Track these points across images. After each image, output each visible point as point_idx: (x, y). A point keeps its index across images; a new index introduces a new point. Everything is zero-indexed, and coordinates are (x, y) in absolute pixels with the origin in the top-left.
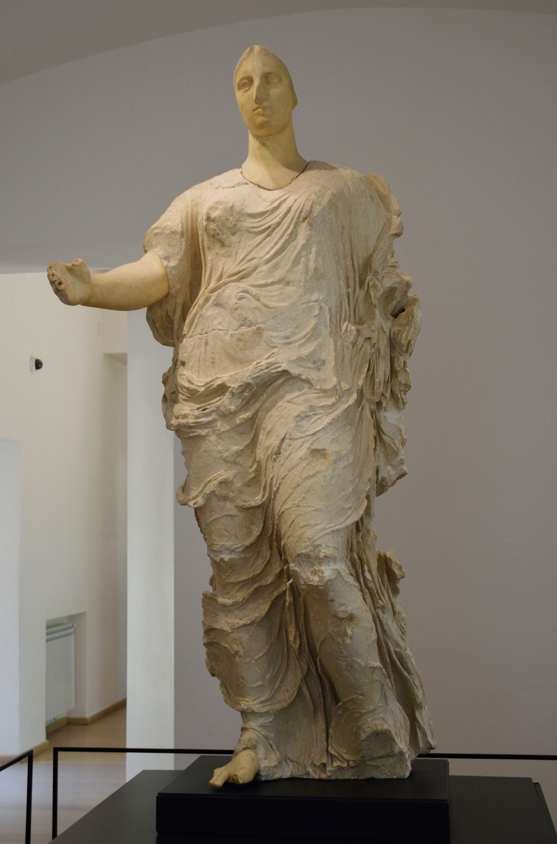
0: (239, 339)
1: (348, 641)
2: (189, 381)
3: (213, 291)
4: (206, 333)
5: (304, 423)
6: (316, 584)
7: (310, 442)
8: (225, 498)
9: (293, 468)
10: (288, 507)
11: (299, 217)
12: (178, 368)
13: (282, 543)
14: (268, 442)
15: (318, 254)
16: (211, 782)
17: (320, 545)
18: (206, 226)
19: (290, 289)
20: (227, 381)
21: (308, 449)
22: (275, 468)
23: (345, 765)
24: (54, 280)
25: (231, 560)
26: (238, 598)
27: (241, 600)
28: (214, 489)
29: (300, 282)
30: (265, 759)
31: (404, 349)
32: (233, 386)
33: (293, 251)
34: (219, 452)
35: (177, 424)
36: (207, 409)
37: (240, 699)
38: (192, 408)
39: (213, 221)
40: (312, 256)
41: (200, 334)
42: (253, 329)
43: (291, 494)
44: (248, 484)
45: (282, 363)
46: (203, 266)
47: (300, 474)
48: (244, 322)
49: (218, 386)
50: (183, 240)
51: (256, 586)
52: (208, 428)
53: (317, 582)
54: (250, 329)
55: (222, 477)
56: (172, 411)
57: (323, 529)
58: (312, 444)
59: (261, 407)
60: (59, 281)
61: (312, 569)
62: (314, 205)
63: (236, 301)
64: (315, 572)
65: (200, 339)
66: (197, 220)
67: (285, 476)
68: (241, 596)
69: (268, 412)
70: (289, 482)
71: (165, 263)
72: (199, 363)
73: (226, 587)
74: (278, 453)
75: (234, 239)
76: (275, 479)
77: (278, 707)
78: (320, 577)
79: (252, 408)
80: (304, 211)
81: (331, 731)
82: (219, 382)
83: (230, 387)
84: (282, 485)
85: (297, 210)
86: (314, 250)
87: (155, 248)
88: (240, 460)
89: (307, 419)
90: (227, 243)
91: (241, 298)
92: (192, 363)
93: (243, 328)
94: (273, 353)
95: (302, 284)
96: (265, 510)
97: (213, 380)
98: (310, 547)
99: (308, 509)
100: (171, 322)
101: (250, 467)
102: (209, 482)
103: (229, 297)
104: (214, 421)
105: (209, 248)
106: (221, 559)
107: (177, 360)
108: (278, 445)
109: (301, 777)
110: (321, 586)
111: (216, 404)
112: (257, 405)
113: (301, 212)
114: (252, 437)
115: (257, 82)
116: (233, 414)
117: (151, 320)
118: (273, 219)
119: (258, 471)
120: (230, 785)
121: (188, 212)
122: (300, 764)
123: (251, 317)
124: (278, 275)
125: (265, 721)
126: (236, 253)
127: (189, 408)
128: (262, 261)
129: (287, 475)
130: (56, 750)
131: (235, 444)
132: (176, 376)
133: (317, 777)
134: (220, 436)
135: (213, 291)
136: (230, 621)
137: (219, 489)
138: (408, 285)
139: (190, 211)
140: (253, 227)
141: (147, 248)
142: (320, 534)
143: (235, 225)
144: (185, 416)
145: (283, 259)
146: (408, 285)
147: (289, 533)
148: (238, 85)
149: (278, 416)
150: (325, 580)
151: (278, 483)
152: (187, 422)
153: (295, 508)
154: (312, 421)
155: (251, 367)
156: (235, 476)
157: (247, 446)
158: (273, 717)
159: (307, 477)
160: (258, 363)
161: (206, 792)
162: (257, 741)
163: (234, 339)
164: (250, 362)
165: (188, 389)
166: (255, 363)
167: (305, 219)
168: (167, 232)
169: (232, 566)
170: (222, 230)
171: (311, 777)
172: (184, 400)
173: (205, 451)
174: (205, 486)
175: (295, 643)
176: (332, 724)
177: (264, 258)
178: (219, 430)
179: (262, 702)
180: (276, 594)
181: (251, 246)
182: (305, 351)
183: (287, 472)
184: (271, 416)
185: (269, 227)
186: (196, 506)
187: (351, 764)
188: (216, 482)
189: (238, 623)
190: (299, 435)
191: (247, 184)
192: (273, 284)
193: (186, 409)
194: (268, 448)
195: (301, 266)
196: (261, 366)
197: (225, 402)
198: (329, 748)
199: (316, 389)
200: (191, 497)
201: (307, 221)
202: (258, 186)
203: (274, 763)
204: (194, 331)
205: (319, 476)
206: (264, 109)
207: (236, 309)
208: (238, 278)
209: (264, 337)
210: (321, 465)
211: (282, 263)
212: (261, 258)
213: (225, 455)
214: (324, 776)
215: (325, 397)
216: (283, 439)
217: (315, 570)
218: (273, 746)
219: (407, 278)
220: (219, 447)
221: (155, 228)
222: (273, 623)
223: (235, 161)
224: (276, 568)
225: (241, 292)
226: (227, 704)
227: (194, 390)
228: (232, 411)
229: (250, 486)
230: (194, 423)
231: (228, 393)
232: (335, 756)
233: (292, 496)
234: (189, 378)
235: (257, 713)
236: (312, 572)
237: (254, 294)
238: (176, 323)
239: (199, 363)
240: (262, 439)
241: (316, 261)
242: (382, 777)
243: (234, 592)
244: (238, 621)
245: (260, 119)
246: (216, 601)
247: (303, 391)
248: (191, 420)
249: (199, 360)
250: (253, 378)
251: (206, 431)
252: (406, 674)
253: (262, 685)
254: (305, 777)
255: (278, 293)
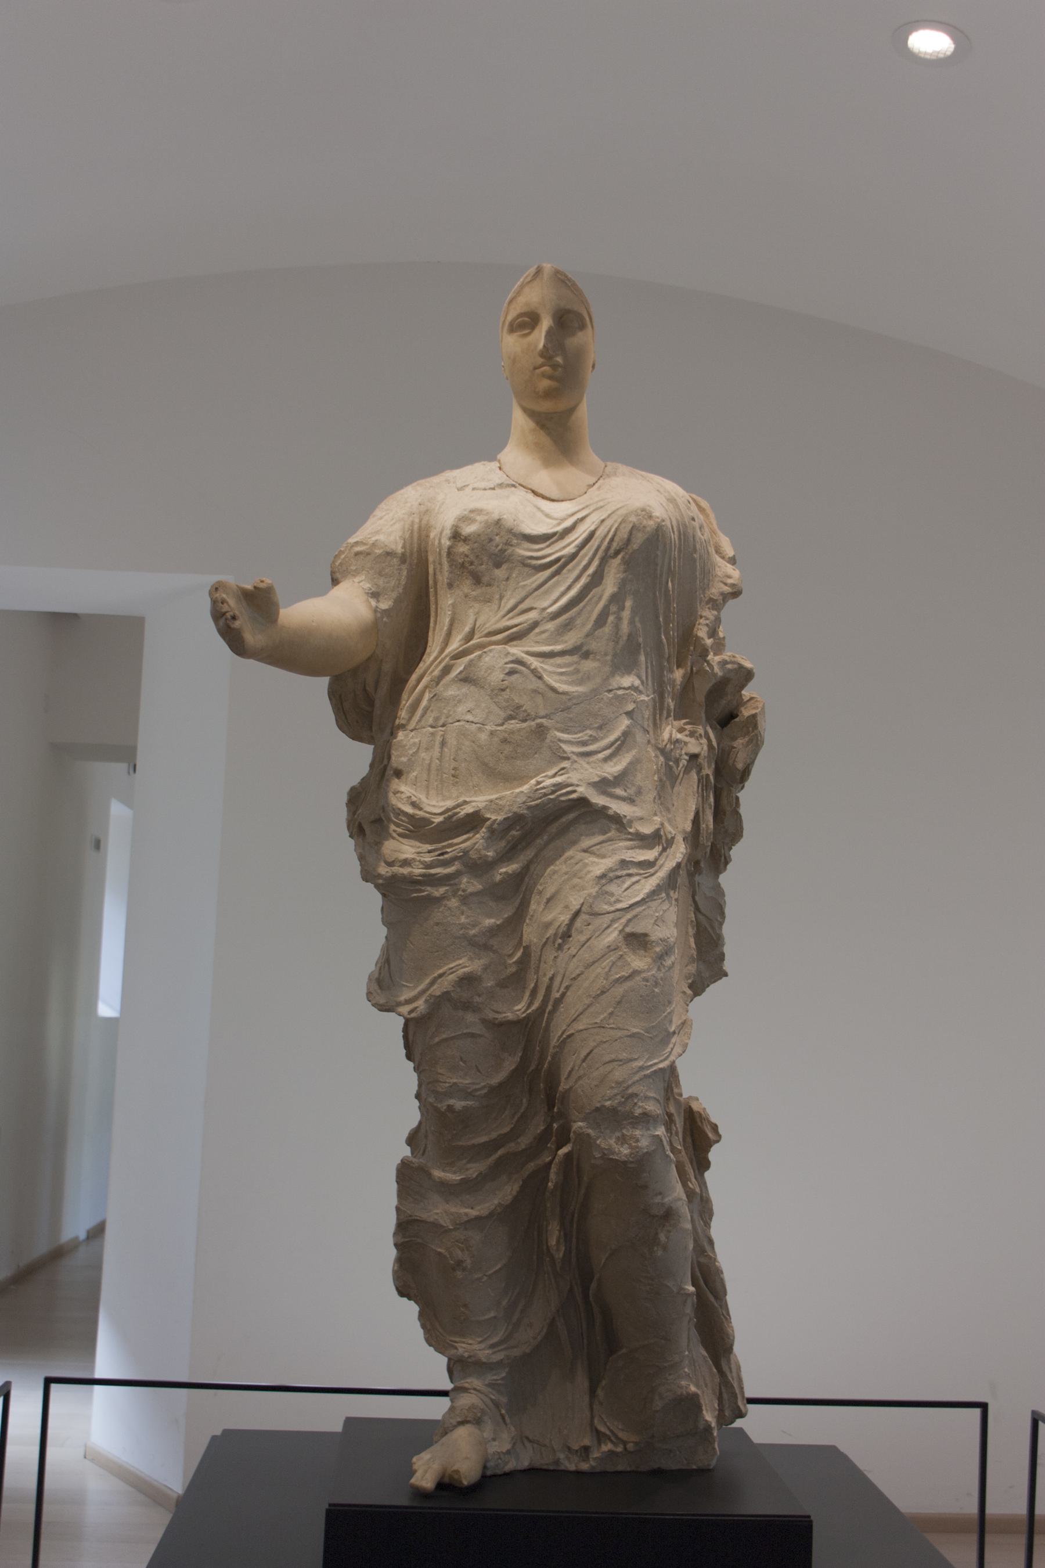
0: (505, 741)
1: (660, 1253)
2: (414, 805)
3: (457, 656)
4: (443, 726)
5: (612, 888)
6: (624, 1158)
7: (623, 921)
8: (467, 1006)
9: (594, 963)
10: (581, 1028)
11: (608, 548)
12: (388, 780)
13: (563, 1086)
14: (547, 915)
15: (634, 611)
16: (413, 1481)
17: (636, 1095)
18: (450, 548)
19: (588, 665)
20: (485, 808)
21: (620, 931)
22: (559, 960)
23: (620, 1449)
24: (224, 610)
25: (466, 1108)
26: (471, 1171)
27: (474, 1176)
28: (450, 988)
29: (606, 655)
30: (494, 1440)
31: (738, 777)
32: (493, 817)
33: (597, 603)
34: (463, 927)
35: (389, 874)
36: (447, 853)
37: (457, 1339)
38: (420, 850)
39: (466, 540)
40: (626, 614)
41: (432, 727)
42: (530, 726)
43: (589, 1006)
44: (502, 984)
45: (578, 785)
46: (433, 614)
47: (607, 974)
48: (515, 713)
49: (468, 815)
50: (404, 567)
51: (500, 1152)
52: (446, 885)
53: (626, 1155)
54: (525, 725)
55: (466, 970)
56: (378, 851)
57: (642, 1068)
58: (626, 925)
59: (536, 856)
60: (231, 613)
61: (618, 1134)
62: (634, 532)
63: (502, 676)
64: (623, 1140)
65: (432, 734)
66: (428, 536)
67: (579, 975)
68: (474, 1169)
69: (549, 866)
70: (586, 984)
71: (373, 603)
72: (429, 774)
73: (451, 1155)
74: (567, 935)
75: (500, 573)
76: (558, 980)
77: (516, 1352)
78: (631, 1147)
79: (522, 857)
80: (617, 539)
81: (600, 1392)
82: (469, 809)
83: (489, 819)
84: (571, 989)
85: (606, 536)
86: (628, 604)
87: (354, 576)
88: (494, 942)
89: (618, 881)
90: (485, 579)
91: (511, 673)
92: (414, 774)
93: (513, 721)
94: (563, 769)
95: (609, 658)
96: (528, 1033)
97: (458, 806)
98: (619, 1097)
99: (619, 1033)
100: (371, 702)
101: (510, 956)
102: (441, 976)
103: (491, 669)
104: (458, 874)
105: (450, 586)
106: (449, 1106)
107: (385, 768)
108: (566, 922)
109: (545, 1467)
110: (632, 1162)
111: (463, 846)
112: (530, 853)
113: (612, 540)
114: (517, 904)
115: (546, 323)
116: (489, 866)
117: (336, 695)
118: (564, 548)
119: (524, 963)
120: (446, 1486)
121: (413, 522)
122: (545, 1446)
123: (528, 706)
124: (571, 639)
125: (495, 1377)
126: (501, 598)
127: (414, 850)
128: (545, 614)
129: (582, 973)
130: (48, 1382)
131: (490, 917)
132: (387, 793)
133: (572, 1467)
134: (465, 900)
135: (457, 656)
136: (453, 1210)
137: (459, 990)
138: (748, 675)
139: (417, 520)
140: (532, 558)
141: (338, 575)
142: (637, 1078)
143: (503, 551)
144: (406, 863)
145: (579, 614)
146: (748, 675)
147: (582, 1072)
148: (511, 324)
149: (566, 874)
150: (640, 1153)
151: (564, 985)
152: (410, 873)
153: (596, 1030)
154: (626, 886)
155: (525, 788)
156: (486, 968)
157: (509, 921)
158: (507, 1370)
159: (618, 980)
160: (539, 783)
161: (403, 1500)
162: (483, 1411)
163: (496, 739)
164: (522, 779)
165: (411, 817)
166: (533, 782)
167: (617, 553)
168: (378, 551)
169: (464, 1121)
170: (487, 556)
171: (563, 1468)
172: (400, 835)
173: (437, 924)
174: (432, 983)
175: (558, 1250)
176: (604, 1383)
177: (550, 610)
178: (464, 891)
179: (493, 1346)
180: (531, 1166)
181: (528, 589)
182: (613, 769)
183: (581, 969)
184: (555, 872)
185: (558, 560)
186: (413, 1015)
187: (630, 1447)
188: (452, 977)
189: (466, 1214)
190: (607, 908)
191: (513, 486)
192: (562, 653)
193: (405, 851)
194: (547, 926)
195: (607, 629)
196: (544, 788)
197: (475, 841)
198: (596, 1421)
199: (630, 833)
200: (402, 998)
201: (620, 556)
202: (533, 492)
203: (506, 1446)
204: (420, 721)
205: (638, 978)
206: (555, 367)
207: (503, 690)
208: (504, 638)
209: (548, 741)
210: (638, 962)
211: (578, 622)
212: (544, 609)
213: (472, 932)
214: (585, 1467)
215: (640, 847)
216: (577, 914)
217: (623, 1135)
218: (507, 1417)
219: (748, 665)
220: (463, 919)
221: (357, 543)
222: (523, 1219)
223: (488, 451)
224: (537, 1126)
225: (512, 662)
226: (430, 1345)
227: (423, 819)
228: (490, 859)
229: (507, 987)
230: (420, 875)
231: (484, 829)
232: (604, 1434)
233: (591, 1009)
234: (414, 799)
235: (484, 1363)
236: (618, 1138)
237: (533, 667)
238: (377, 704)
239: (429, 774)
240: (534, 911)
241: (632, 622)
242: (674, 1467)
243: (464, 1161)
244: (467, 1210)
245: (546, 383)
246: (429, 1175)
247: (609, 835)
248: (417, 871)
249: (429, 770)
250: (529, 808)
251: (442, 890)
252: (712, 1299)
253: (495, 1317)
254: (551, 1468)
255: (571, 669)
